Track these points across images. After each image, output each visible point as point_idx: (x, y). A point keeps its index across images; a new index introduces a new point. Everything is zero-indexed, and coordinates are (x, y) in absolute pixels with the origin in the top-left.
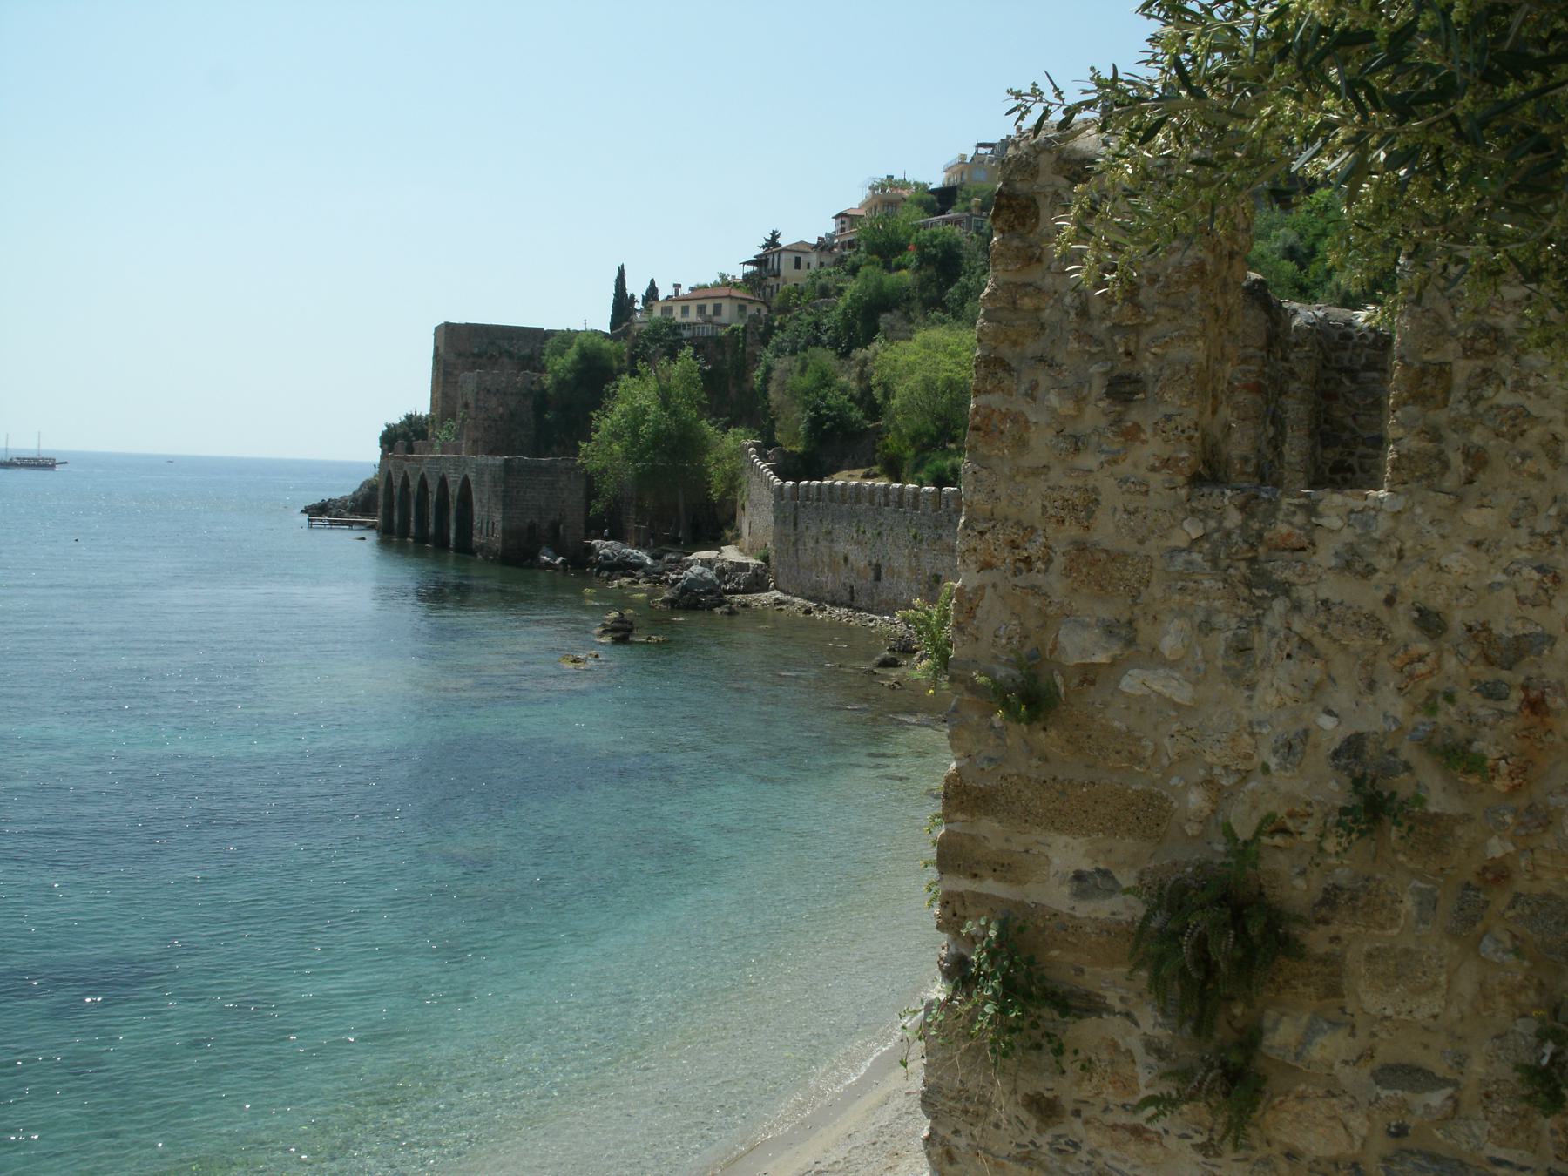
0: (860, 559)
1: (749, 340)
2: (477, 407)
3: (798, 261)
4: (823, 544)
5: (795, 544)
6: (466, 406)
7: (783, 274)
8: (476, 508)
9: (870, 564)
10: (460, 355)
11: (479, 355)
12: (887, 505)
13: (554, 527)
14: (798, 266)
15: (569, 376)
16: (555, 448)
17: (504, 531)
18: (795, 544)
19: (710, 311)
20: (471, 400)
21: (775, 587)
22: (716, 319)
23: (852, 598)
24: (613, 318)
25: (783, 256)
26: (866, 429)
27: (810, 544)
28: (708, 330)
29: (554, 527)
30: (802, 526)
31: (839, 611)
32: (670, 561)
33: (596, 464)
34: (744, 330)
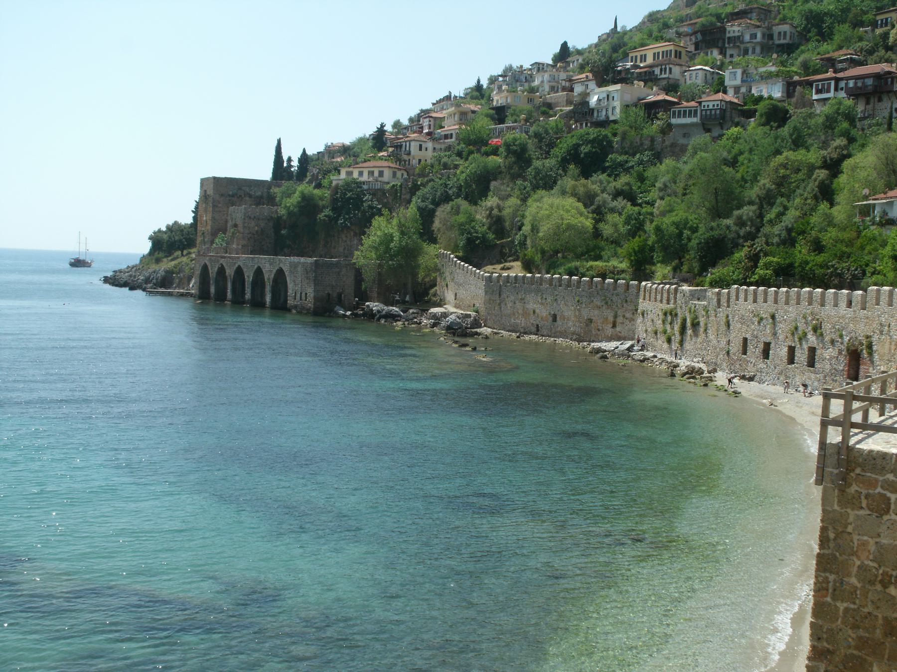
0: (544, 312)
1: (404, 191)
2: (244, 227)
3: (421, 146)
4: (519, 305)
5: (500, 304)
6: (236, 226)
7: (412, 153)
8: (290, 286)
9: (550, 314)
10: (222, 195)
11: (233, 196)
12: (560, 286)
13: (340, 295)
14: (420, 149)
15: (296, 210)
16: (286, 250)
17: (315, 297)
18: (500, 304)
19: (376, 174)
20: (240, 223)
21: (485, 326)
22: (380, 179)
23: (538, 330)
24: (274, 169)
25: (413, 144)
26: (496, 244)
27: (509, 305)
28: (378, 186)
29: (340, 295)
30: (504, 295)
31: (533, 337)
32: (413, 313)
33: (362, 261)
34: (401, 186)
